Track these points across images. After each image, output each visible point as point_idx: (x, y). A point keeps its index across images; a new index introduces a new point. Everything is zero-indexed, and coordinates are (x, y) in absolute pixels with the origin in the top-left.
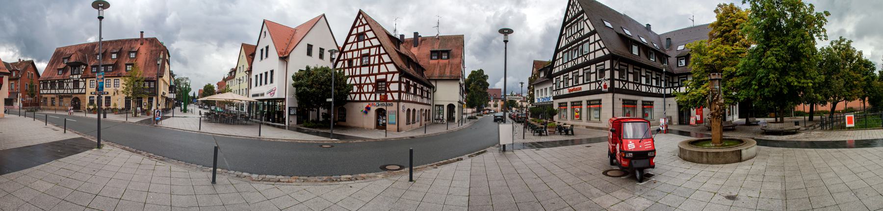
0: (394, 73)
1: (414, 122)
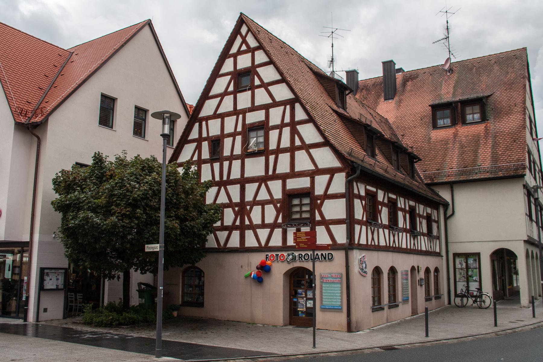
0: (331, 172)
1: (393, 304)
